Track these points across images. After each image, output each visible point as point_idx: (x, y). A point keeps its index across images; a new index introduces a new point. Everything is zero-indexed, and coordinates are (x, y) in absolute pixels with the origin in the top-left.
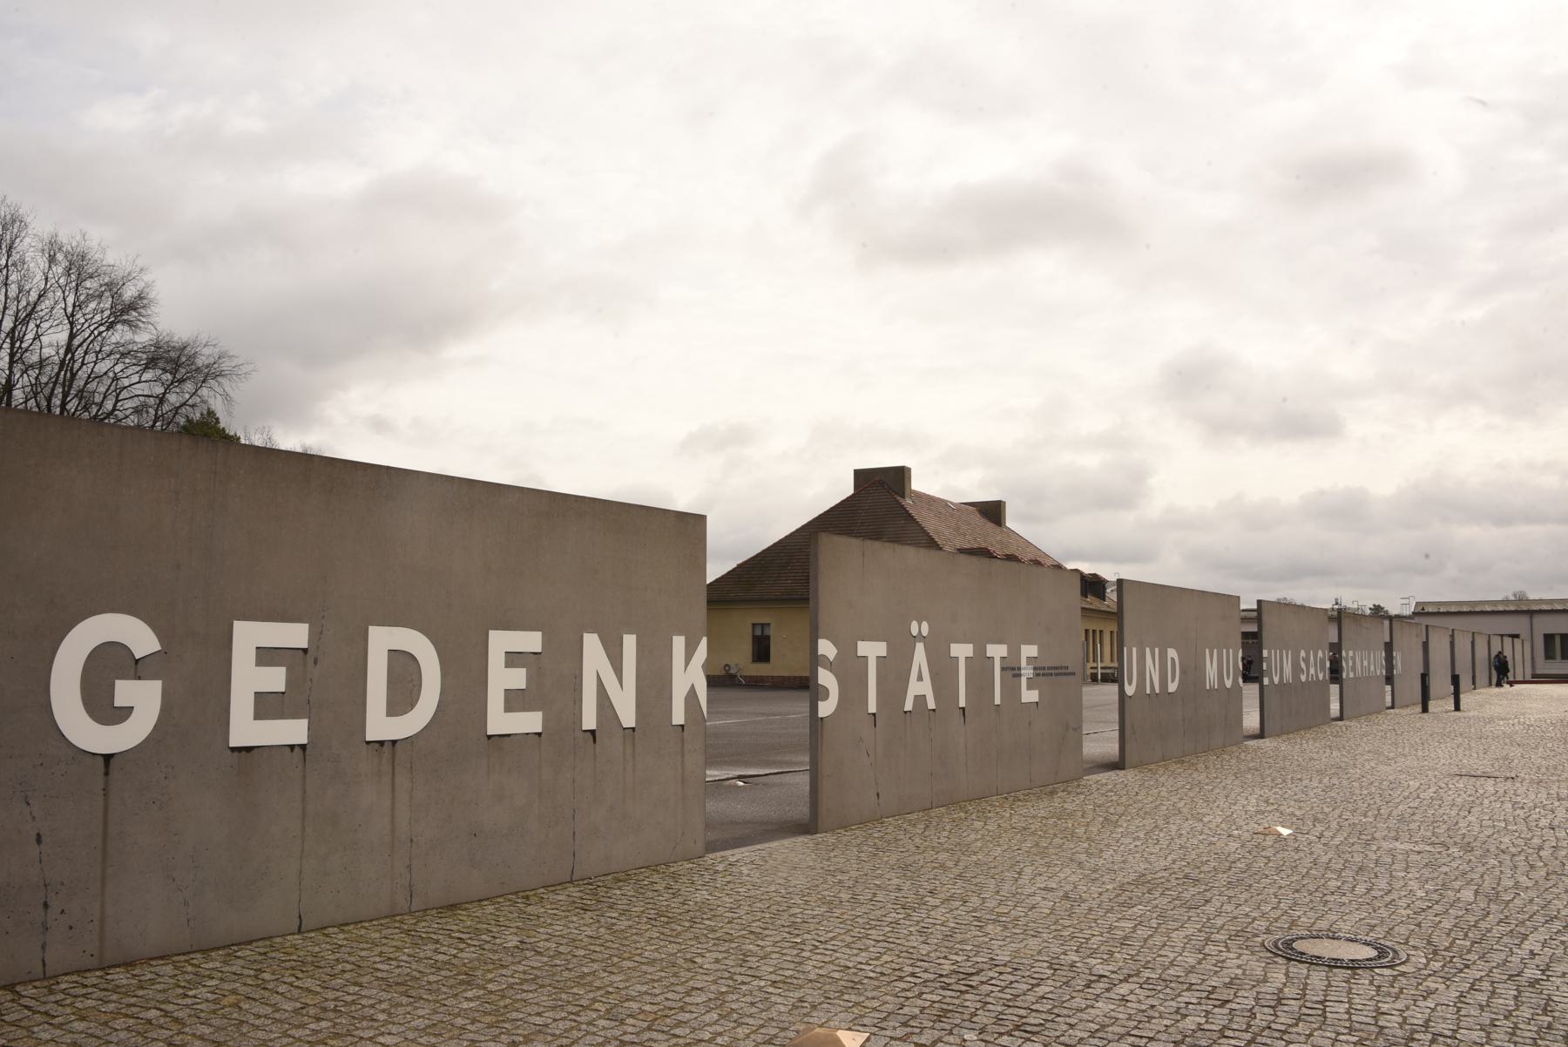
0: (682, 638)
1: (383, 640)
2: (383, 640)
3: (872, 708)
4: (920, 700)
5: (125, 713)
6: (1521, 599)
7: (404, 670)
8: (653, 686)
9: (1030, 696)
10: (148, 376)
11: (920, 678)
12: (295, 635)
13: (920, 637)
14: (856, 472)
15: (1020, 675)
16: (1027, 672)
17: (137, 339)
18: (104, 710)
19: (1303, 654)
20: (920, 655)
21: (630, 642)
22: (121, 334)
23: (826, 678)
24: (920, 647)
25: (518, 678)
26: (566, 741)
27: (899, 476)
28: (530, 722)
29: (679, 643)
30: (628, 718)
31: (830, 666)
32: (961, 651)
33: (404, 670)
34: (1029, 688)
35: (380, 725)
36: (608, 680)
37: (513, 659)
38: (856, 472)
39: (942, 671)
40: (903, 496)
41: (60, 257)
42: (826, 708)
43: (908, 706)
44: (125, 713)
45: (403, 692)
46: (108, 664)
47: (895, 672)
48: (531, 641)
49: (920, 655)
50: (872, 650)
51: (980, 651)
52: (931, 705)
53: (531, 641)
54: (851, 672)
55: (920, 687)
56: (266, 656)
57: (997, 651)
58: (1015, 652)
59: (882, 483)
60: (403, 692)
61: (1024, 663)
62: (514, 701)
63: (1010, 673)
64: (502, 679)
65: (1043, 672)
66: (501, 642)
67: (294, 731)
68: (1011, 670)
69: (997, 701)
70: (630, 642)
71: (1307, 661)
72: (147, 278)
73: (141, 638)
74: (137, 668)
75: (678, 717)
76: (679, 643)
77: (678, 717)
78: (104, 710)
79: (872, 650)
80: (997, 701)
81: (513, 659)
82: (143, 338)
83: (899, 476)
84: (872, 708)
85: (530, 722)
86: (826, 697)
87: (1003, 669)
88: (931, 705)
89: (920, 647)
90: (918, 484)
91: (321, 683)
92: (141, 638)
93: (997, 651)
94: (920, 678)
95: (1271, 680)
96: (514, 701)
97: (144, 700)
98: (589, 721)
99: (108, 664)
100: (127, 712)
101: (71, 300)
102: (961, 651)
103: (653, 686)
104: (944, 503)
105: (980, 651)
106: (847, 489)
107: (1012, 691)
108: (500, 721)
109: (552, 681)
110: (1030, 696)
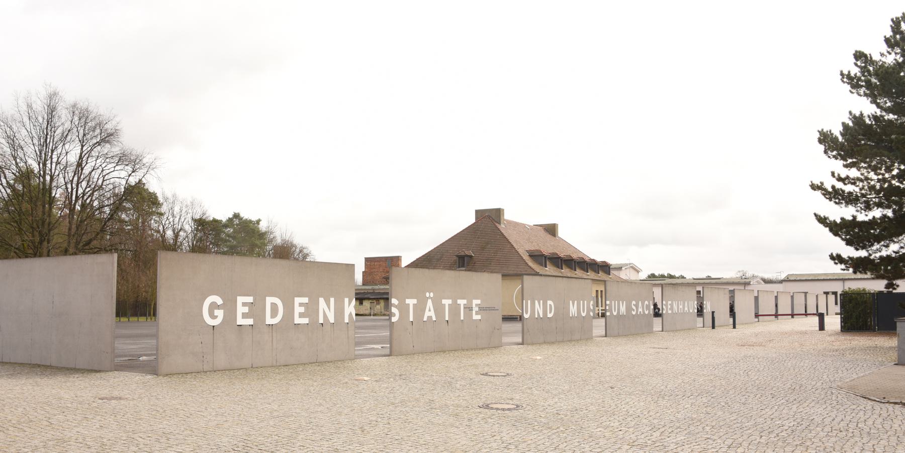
1: (269, 300)
2: (269, 300)
3: (411, 319)
4: (430, 318)
5: (216, 317)
6: (709, 278)
7: (274, 307)
8: (339, 312)
9: (476, 317)
10: (118, 168)
12: (250, 299)
13: (430, 297)
14: (477, 212)
16: (475, 309)
17: (113, 150)
18: (213, 317)
20: (430, 303)
21: (332, 300)
22: (106, 148)
23: (394, 310)
24: (430, 301)
25: (302, 310)
26: (316, 327)
27: (498, 212)
29: (346, 300)
31: (396, 307)
32: (447, 302)
33: (274, 307)
35: (269, 321)
36: (326, 310)
38: (477, 212)
39: (439, 309)
40: (500, 223)
41: (76, 112)
42: (394, 319)
43: (425, 319)
44: (216, 317)
45: (274, 314)
46: (213, 306)
47: (420, 309)
48: (305, 300)
49: (430, 303)
50: (411, 302)
51: (455, 302)
53: (305, 300)
54: (404, 309)
56: (244, 304)
57: (462, 302)
59: (489, 217)
60: (274, 314)
61: (474, 306)
62: (301, 315)
64: (298, 310)
65: (481, 309)
66: (298, 300)
67: (250, 321)
68: (469, 308)
70: (332, 300)
72: (117, 119)
73: (219, 301)
74: (218, 307)
75: (347, 320)
76: (346, 300)
77: (347, 320)
78: (213, 317)
79: (411, 302)
81: (244, 304)
82: (116, 150)
83: (498, 212)
84: (411, 319)
85: (305, 321)
86: (395, 315)
88: (434, 319)
89: (430, 301)
90: (508, 216)
91: (256, 310)
92: (219, 301)
95: (611, 313)
97: (220, 313)
98: (321, 321)
99: (213, 306)
101: (81, 132)
102: (447, 302)
103: (339, 312)
104: (524, 226)
105: (455, 302)
106: (472, 220)
108: (298, 320)
109: (311, 310)
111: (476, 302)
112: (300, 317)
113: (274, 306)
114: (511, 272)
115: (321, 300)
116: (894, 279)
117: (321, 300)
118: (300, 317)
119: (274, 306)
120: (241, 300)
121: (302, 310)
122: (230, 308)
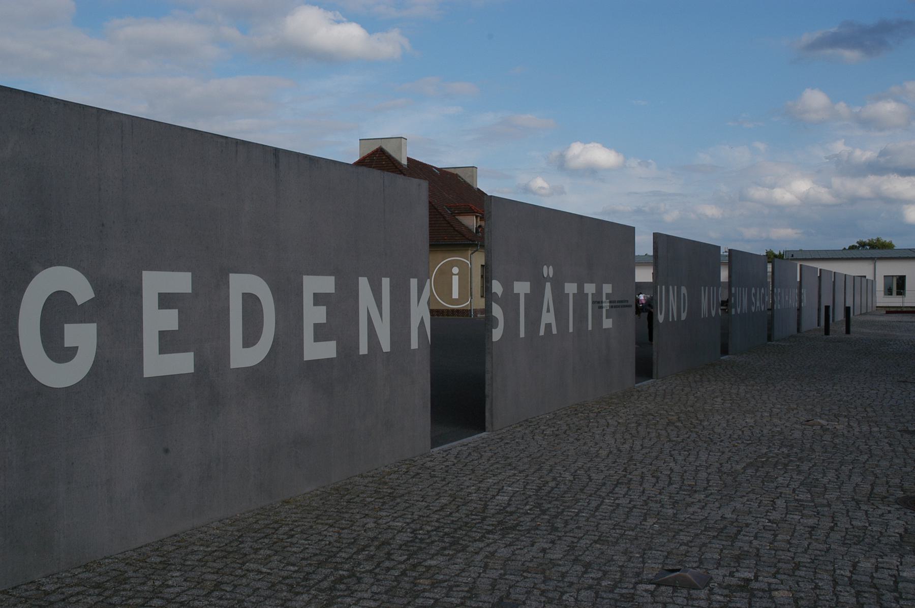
0: (416, 280)
1: (242, 284)
2: (242, 284)
4: (548, 326)
11: (548, 311)
13: (548, 279)
15: (601, 307)
16: (606, 305)
18: (60, 353)
19: (753, 291)
21: (386, 282)
25: (170, 320)
28: (182, 363)
30: (386, 347)
34: (607, 317)
37: (166, 301)
46: (59, 309)
48: (180, 282)
51: (599, 290)
52: (554, 331)
53: (180, 282)
55: (548, 317)
57: (590, 289)
58: (599, 290)
62: (321, 333)
63: (597, 305)
69: (590, 328)
70: (386, 282)
71: (755, 295)
73: (81, 289)
74: (82, 314)
77: (542, 333)
78: (60, 353)
79: (522, 288)
80: (590, 328)
81: (166, 301)
85: (182, 363)
87: (593, 302)
88: (554, 331)
91: (200, 323)
92: (81, 289)
93: (590, 289)
94: (548, 311)
96: (321, 333)
97: (82, 336)
99: (59, 309)
100: (73, 351)
102: (571, 288)
107: (598, 320)
110: (607, 323)
111: (607, 288)
112: (317, 339)
113: (251, 302)
114: (817, 284)
115: (364, 283)
116: (460, 214)
117: (364, 283)
118: (317, 339)
119: (251, 302)
120: (156, 283)
121: (170, 320)
122: (115, 308)
